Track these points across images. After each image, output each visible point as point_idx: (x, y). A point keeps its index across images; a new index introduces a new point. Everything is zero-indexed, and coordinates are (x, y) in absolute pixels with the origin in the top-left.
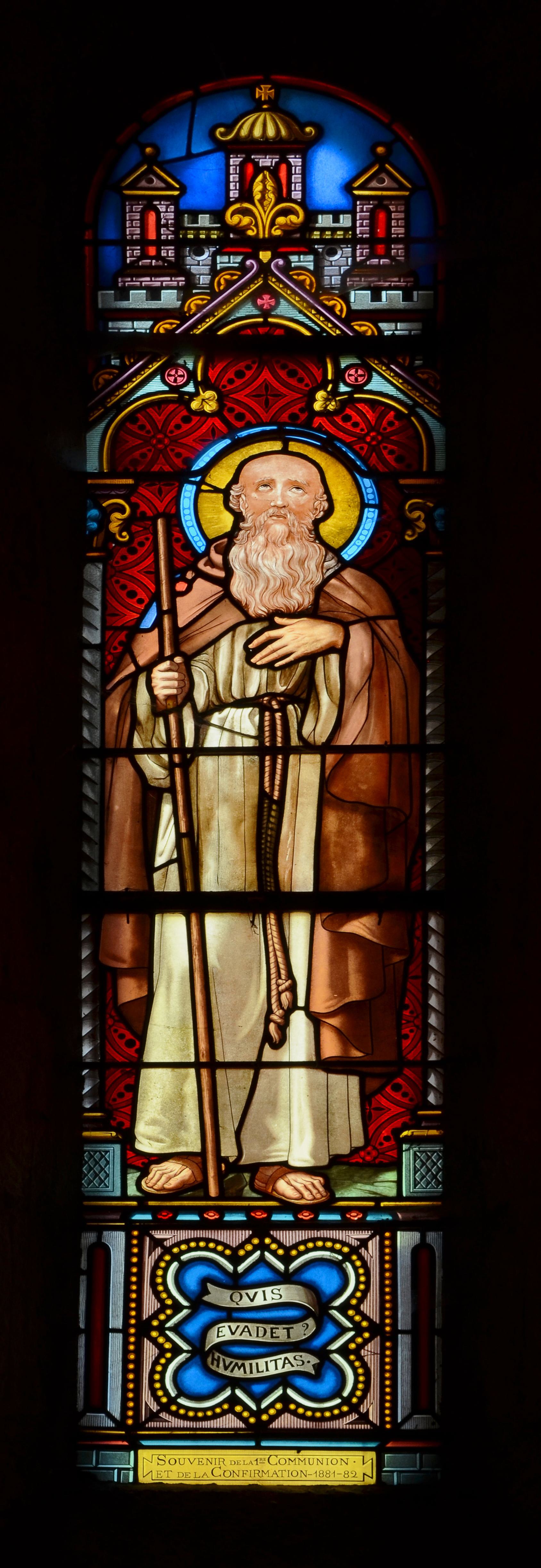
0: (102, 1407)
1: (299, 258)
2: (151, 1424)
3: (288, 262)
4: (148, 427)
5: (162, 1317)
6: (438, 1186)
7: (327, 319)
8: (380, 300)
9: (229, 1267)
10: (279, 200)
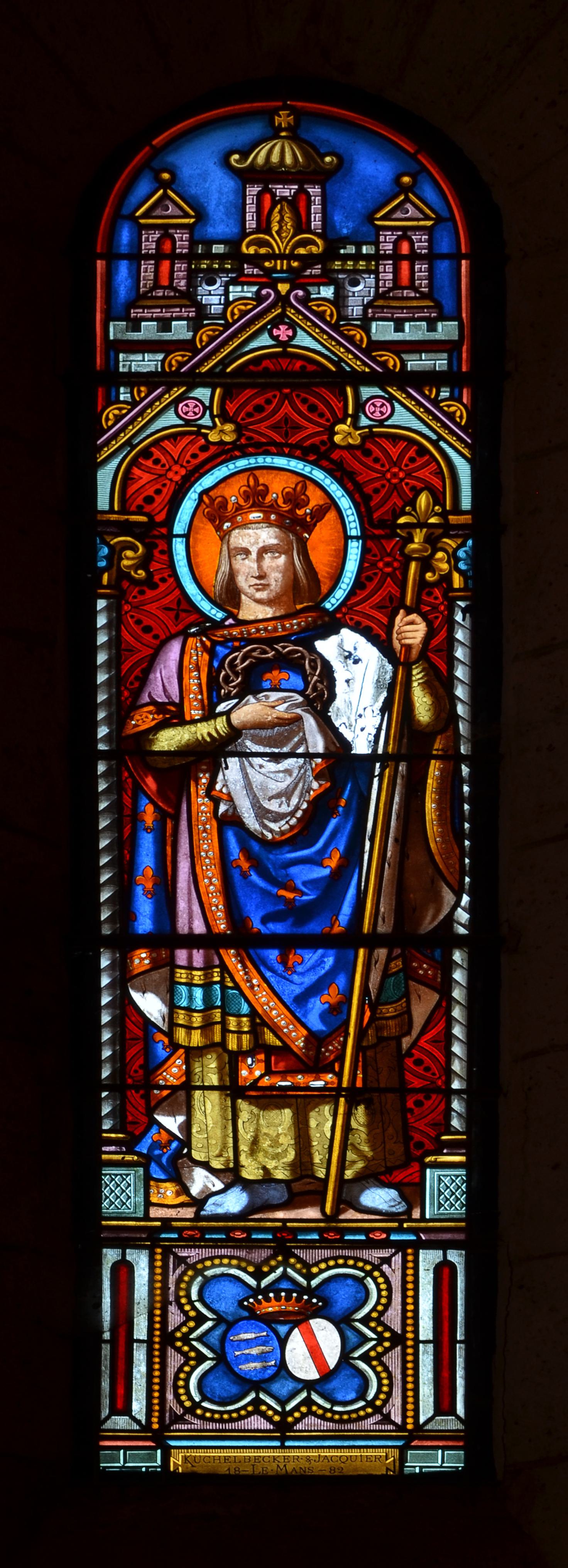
0: (127, 1410)
3: (308, 293)
4: (163, 460)
5: (380, 1349)
6: (461, 1208)
7: (348, 351)
8: (403, 330)
9: (262, 1396)
10: (298, 230)
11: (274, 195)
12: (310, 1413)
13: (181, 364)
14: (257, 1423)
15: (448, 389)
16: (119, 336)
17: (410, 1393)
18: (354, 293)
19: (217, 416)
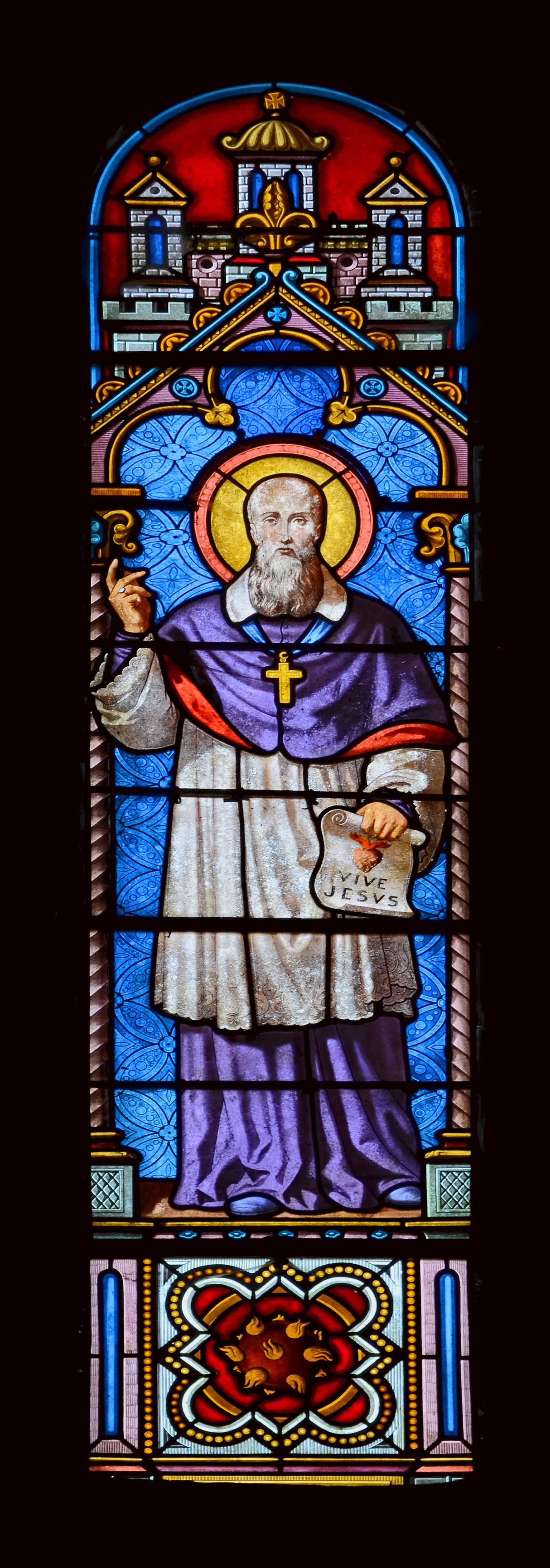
0: (119, 1434)
1: (312, 269)
2: (169, 1451)
3: (300, 274)
8: (398, 310)
11: (264, 176)
12: (308, 1435)
13: (177, 346)
14: (251, 1446)
15: (442, 369)
16: (113, 317)
17: (413, 1405)
18: (346, 272)
19: (212, 395)
